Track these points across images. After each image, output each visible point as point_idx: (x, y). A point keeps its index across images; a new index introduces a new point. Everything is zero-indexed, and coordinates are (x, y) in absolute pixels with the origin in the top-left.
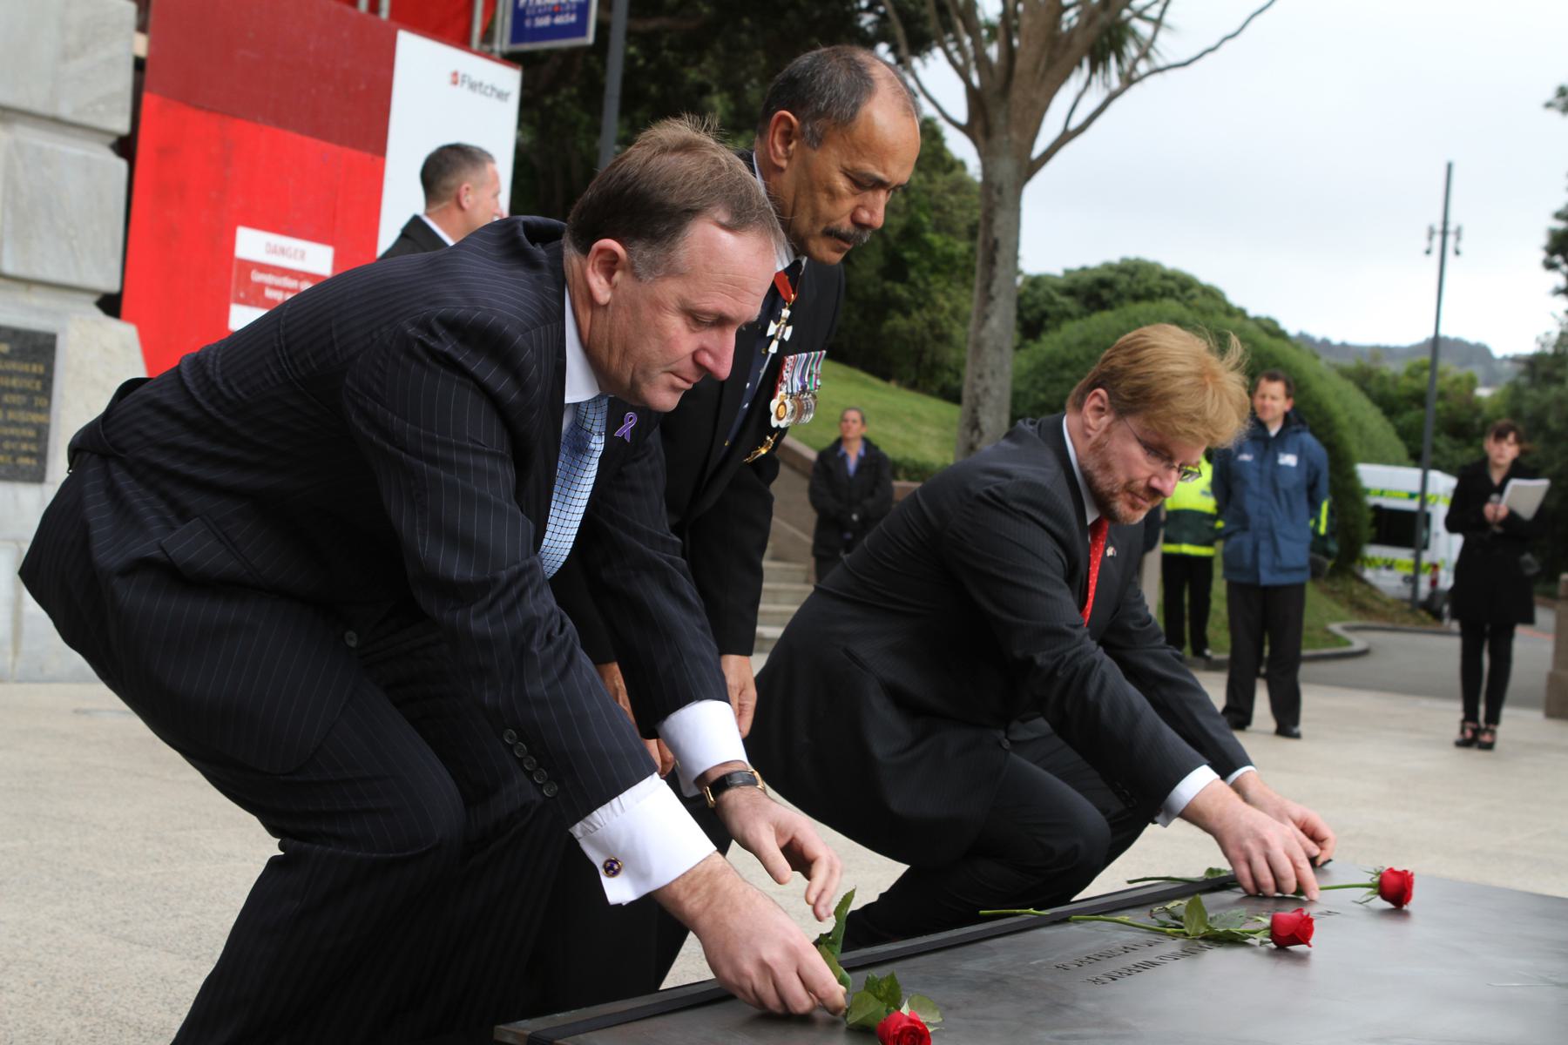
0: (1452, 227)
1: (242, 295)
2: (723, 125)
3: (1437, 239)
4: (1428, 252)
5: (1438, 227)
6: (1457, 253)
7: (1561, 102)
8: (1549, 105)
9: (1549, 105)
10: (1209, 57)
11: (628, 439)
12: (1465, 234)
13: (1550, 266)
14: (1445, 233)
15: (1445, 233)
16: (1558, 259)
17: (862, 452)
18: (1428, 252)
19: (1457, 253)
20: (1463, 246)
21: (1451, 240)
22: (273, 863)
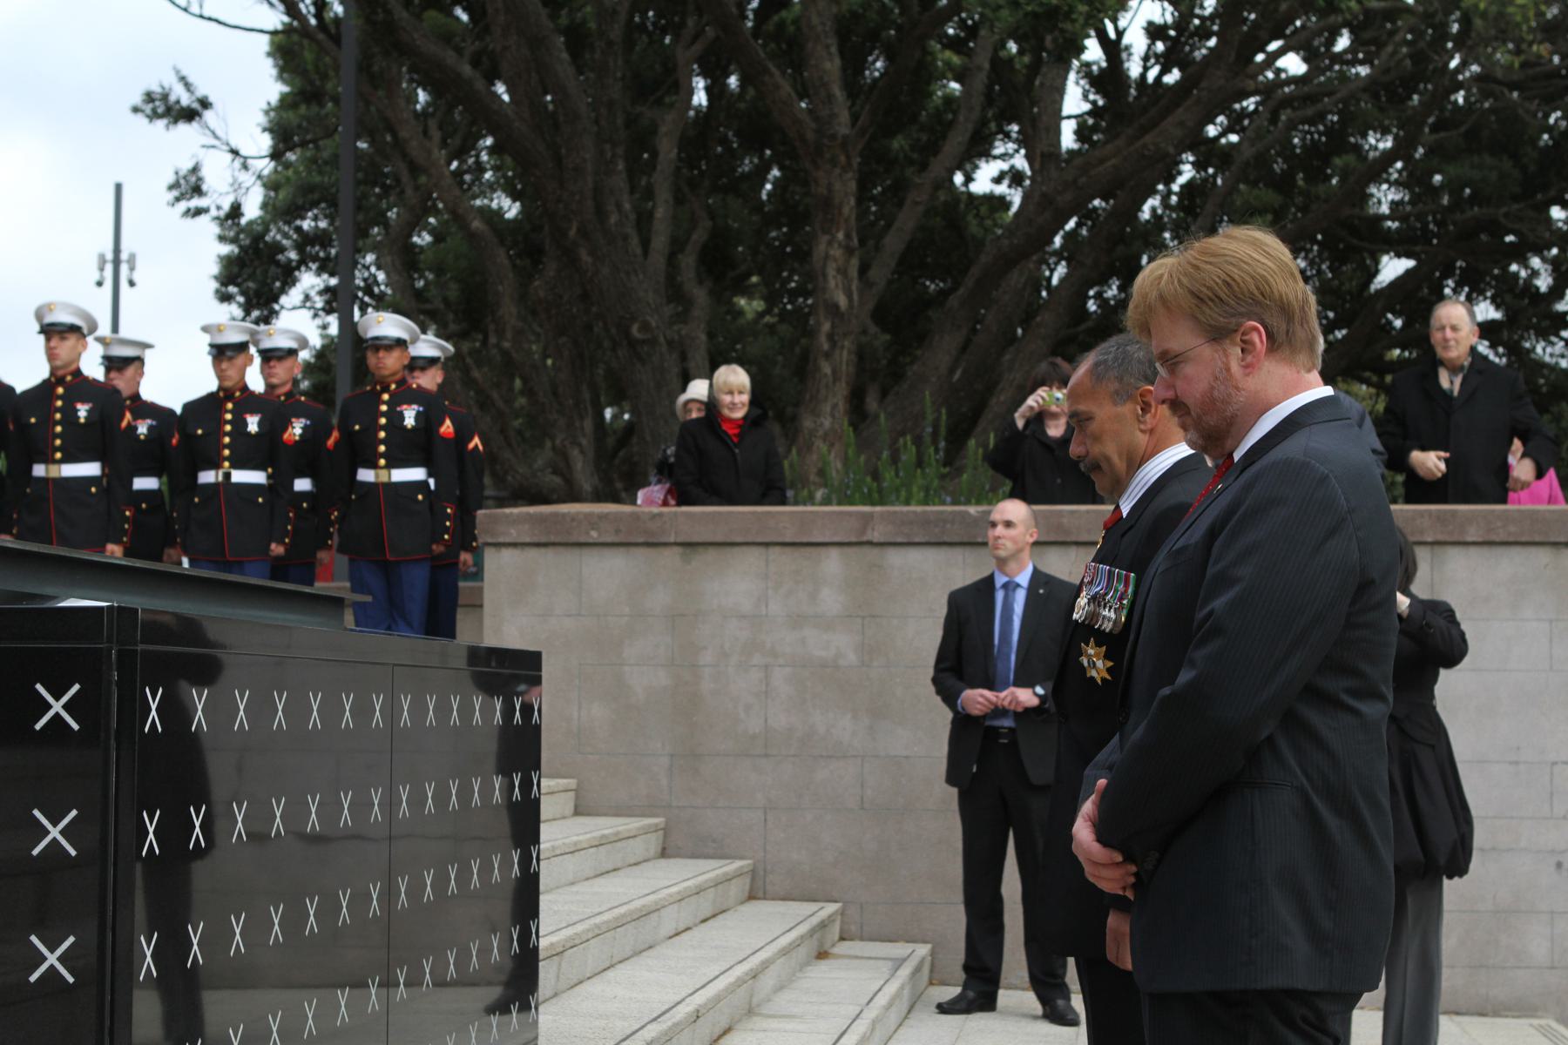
0: (124, 256)
1: (1431, 462)
2: (677, 93)
3: (109, 268)
4: (100, 284)
5: (110, 256)
6: (132, 284)
7: (148, 108)
8: (136, 110)
9: (136, 110)
10: (221, 19)
11: (1110, 664)
12: (139, 263)
13: (225, 298)
14: (117, 262)
15: (117, 262)
16: (232, 289)
17: (1120, 15)
18: (100, 284)
19: (132, 284)
20: (136, 277)
21: (124, 268)
22: (1450, 877)
